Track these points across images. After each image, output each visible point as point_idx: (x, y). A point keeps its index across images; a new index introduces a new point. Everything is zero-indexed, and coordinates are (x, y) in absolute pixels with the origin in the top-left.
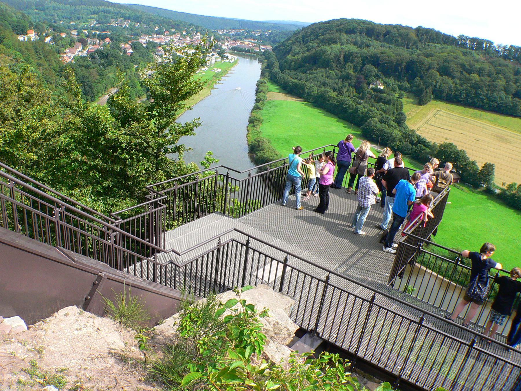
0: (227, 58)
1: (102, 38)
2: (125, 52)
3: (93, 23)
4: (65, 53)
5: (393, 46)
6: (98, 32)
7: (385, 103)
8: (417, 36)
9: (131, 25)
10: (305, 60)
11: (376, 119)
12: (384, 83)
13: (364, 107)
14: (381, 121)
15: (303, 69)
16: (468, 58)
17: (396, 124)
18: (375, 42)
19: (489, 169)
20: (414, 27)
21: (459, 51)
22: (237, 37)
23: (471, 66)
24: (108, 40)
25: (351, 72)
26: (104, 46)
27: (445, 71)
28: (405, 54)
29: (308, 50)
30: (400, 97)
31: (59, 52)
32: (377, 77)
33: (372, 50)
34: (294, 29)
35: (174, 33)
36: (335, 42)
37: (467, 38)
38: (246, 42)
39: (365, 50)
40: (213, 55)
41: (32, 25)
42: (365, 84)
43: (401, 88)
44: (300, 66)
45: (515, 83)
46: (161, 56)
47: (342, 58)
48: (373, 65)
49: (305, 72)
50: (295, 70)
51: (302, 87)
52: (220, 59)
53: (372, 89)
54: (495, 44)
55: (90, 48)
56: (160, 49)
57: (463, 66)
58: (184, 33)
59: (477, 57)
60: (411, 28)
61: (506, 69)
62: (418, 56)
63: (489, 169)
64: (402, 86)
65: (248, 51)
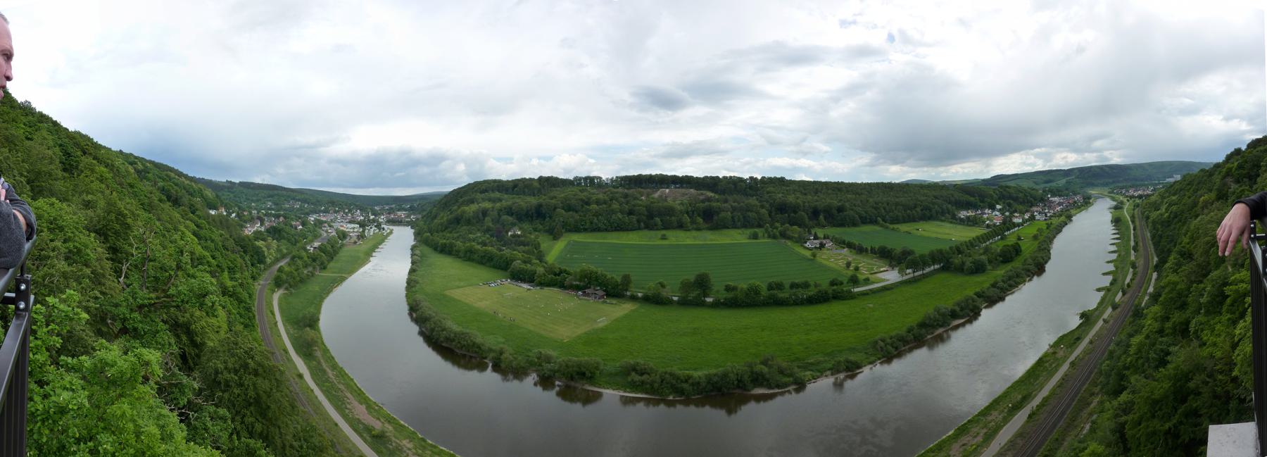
0: (383, 229)
1: (277, 216)
2: (296, 228)
3: (269, 204)
4: (247, 228)
5: (521, 196)
6: (273, 212)
7: (524, 246)
8: (540, 184)
9: (301, 206)
10: (450, 222)
11: (519, 261)
12: (520, 229)
13: (507, 252)
14: (525, 262)
15: (449, 229)
16: (585, 193)
17: (571, 213)
18: (506, 196)
19: (627, 280)
20: (536, 178)
21: (576, 189)
22: (390, 211)
23: (589, 199)
24: (281, 219)
25: (490, 224)
26: (279, 223)
27: (569, 208)
28: (533, 201)
29: (451, 214)
30: (537, 237)
31: (242, 226)
32: (513, 225)
33: (504, 203)
34: (438, 198)
35: (338, 211)
36: (473, 202)
37: (580, 179)
38: (399, 213)
39: (498, 205)
40: (371, 228)
41: (223, 203)
42: (504, 233)
43: (535, 230)
44: (446, 228)
45: (626, 204)
46: (327, 231)
47: (481, 215)
48: (508, 215)
49: (451, 232)
50: (442, 231)
51: (452, 246)
52: (378, 231)
53: (511, 235)
54: (604, 178)
55: (267, 224)
56: (326, 225)
57: (582, 200)
58: (347, 211)
59: (592, 191)
60: (534, 179)
61: (617, 195)
62: (544, 200)
63: (627, 280)
64: (536, 228)
65: (401, 222)
